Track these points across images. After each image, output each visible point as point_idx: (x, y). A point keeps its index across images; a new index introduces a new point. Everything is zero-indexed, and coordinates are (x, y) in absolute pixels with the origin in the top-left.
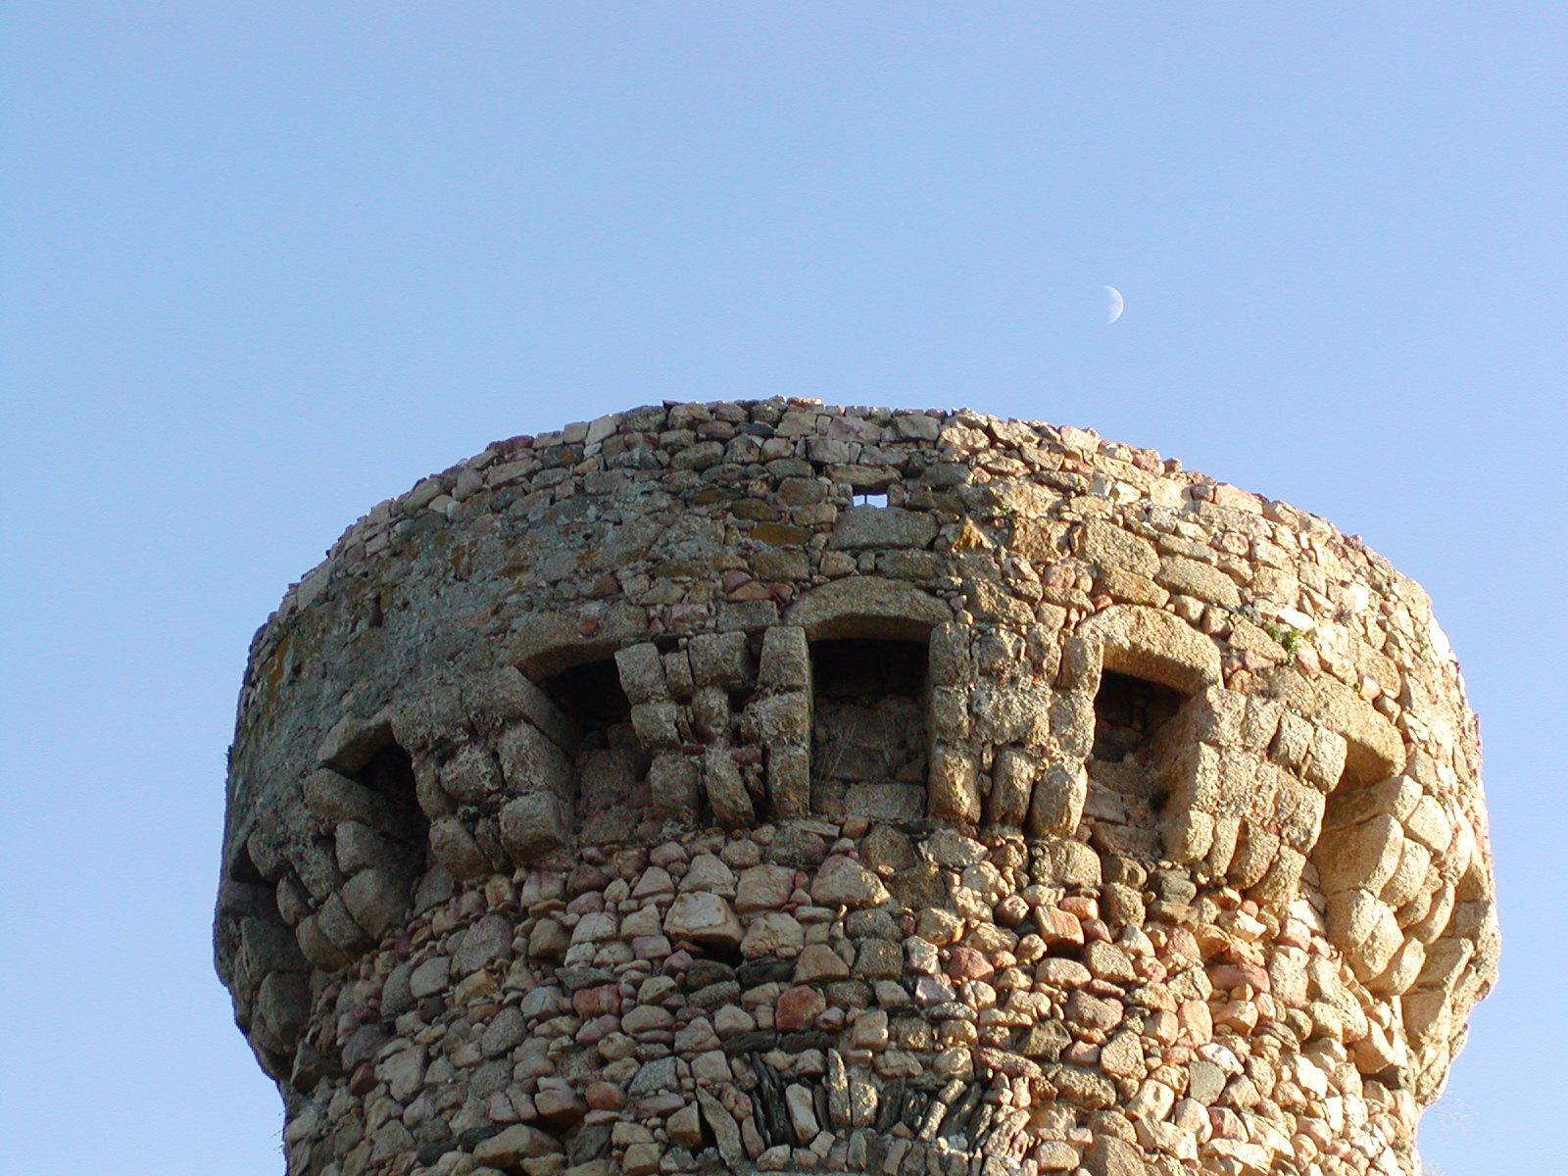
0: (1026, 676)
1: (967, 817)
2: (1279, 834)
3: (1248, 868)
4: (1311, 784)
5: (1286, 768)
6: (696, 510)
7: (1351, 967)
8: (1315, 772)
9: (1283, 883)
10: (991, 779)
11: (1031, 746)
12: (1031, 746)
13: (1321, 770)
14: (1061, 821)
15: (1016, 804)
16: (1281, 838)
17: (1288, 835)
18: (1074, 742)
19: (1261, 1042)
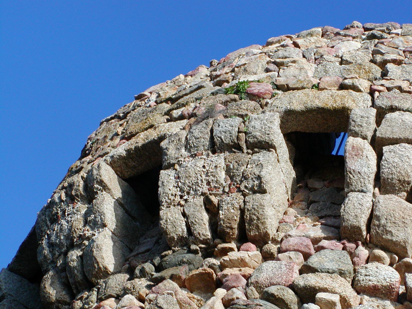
0: (68, 206)
1: (58, 301)
2: (239, 190)
3: (222, 222)
4: (256, 150)
5: (231, 151)
6: (150, 228)
7: (377, 246)
8: (251, 140)
9: (255, 218)
10: (136, 276)
11: (75, 240)
12: (75, 240)
13: (255, 137)
14: (95, 267)
15: (74, 276)
16: (242, 191)
17: (246, 187)
18: (96, 221)
19: (43, 301)
